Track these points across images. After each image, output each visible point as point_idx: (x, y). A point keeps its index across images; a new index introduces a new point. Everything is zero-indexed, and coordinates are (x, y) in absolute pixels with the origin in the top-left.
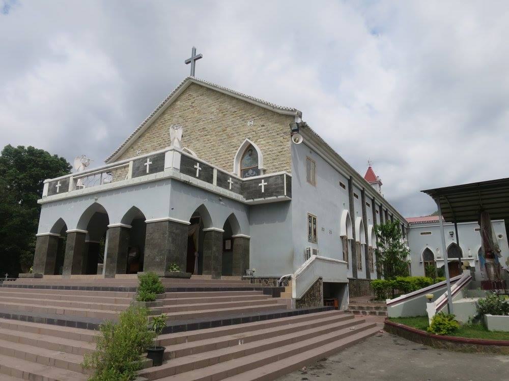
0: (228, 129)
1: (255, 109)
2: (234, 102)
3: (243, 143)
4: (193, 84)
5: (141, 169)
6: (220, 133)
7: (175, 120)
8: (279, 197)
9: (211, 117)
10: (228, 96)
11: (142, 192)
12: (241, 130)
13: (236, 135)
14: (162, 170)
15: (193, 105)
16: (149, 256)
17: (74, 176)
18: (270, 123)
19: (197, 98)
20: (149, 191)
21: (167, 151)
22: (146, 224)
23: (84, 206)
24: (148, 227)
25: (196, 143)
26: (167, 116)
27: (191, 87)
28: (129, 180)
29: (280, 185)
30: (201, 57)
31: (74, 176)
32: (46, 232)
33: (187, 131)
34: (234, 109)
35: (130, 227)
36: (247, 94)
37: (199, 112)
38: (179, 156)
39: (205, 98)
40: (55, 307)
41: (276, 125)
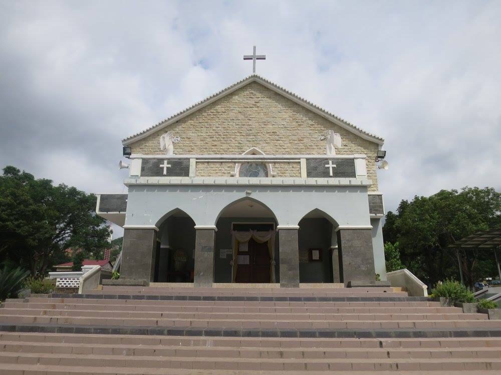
0: (305, 139)
1: (336, 128)
2: (310, 115)
3: (250, 149)
4: (255, 82)
5: (320, 169)
6: (296, 142)
7: (232, 115)
8: (378, 215)
9: (282, 123)
10: (303, 108)
11: (325, 194)
12: (322, 145)
13: (315, 147)
14: (163, 164)
15: (258, 104)
16: (350, 264)
17: (197, 159)
18: (353, 145)
19: (263, 99)
20: (337, 194)
21: (356, 158)
22: (195, 230)
23: (222, 201)
24: (197, 232)
25: (265, 145)
26: (219, 108)
27: (253, 85)
28: (303, 179)
29: (378, 204)
30: (265, 59)
31: (197, 159)
32: (151, 224)
33: (251, 130)
34: (311, 122)
35: (158, 230)
36: (208, 95)
37: (265, 114)
38: (305, 160)
39: (274, 103)
40: (310, 321)
41: (360, 147)
